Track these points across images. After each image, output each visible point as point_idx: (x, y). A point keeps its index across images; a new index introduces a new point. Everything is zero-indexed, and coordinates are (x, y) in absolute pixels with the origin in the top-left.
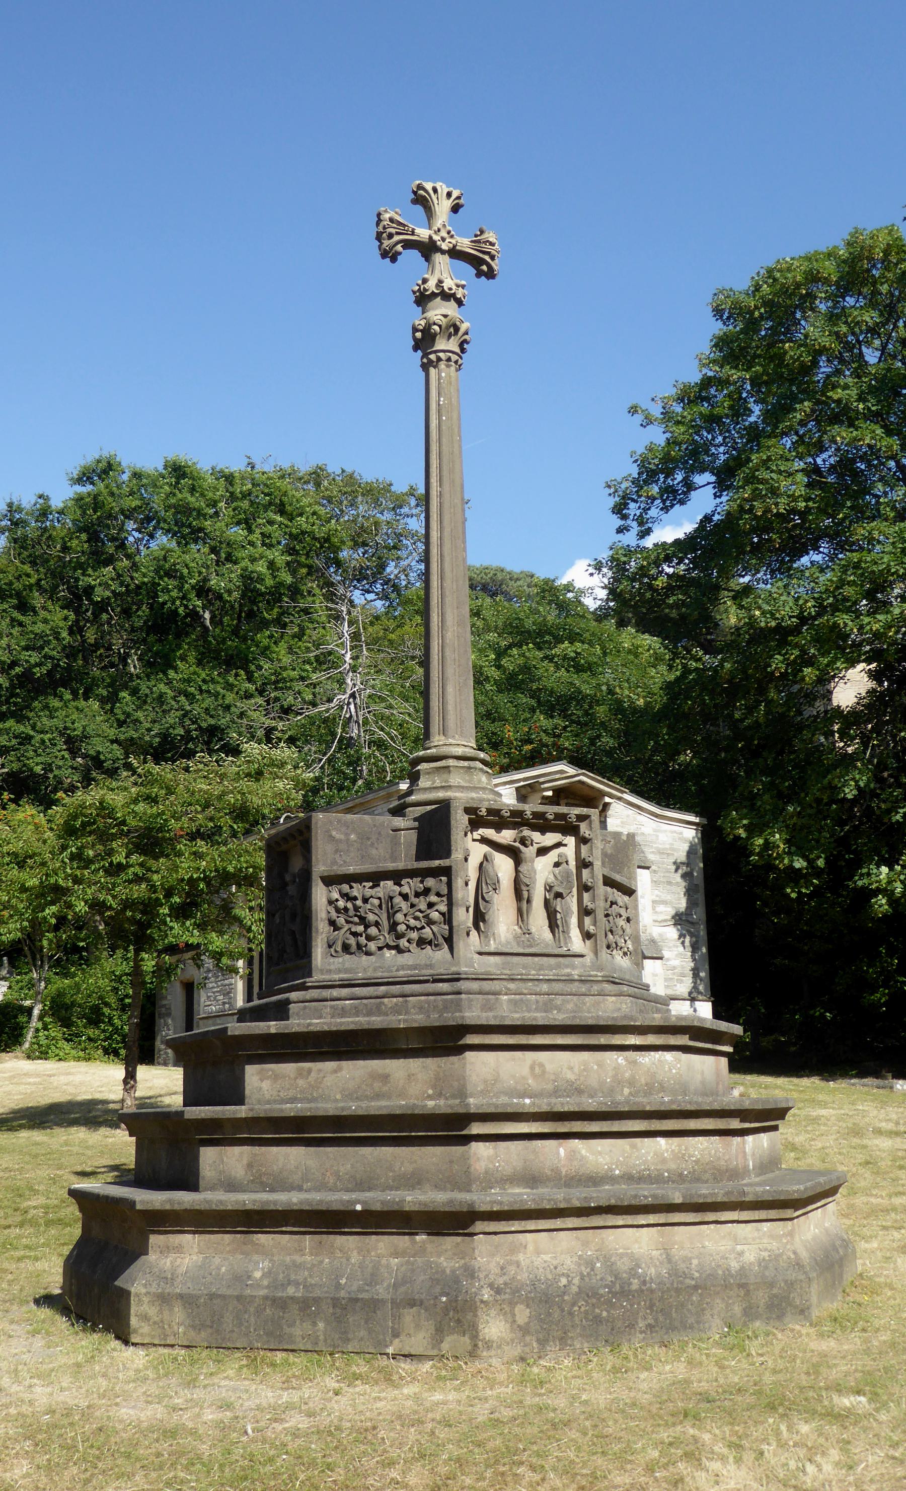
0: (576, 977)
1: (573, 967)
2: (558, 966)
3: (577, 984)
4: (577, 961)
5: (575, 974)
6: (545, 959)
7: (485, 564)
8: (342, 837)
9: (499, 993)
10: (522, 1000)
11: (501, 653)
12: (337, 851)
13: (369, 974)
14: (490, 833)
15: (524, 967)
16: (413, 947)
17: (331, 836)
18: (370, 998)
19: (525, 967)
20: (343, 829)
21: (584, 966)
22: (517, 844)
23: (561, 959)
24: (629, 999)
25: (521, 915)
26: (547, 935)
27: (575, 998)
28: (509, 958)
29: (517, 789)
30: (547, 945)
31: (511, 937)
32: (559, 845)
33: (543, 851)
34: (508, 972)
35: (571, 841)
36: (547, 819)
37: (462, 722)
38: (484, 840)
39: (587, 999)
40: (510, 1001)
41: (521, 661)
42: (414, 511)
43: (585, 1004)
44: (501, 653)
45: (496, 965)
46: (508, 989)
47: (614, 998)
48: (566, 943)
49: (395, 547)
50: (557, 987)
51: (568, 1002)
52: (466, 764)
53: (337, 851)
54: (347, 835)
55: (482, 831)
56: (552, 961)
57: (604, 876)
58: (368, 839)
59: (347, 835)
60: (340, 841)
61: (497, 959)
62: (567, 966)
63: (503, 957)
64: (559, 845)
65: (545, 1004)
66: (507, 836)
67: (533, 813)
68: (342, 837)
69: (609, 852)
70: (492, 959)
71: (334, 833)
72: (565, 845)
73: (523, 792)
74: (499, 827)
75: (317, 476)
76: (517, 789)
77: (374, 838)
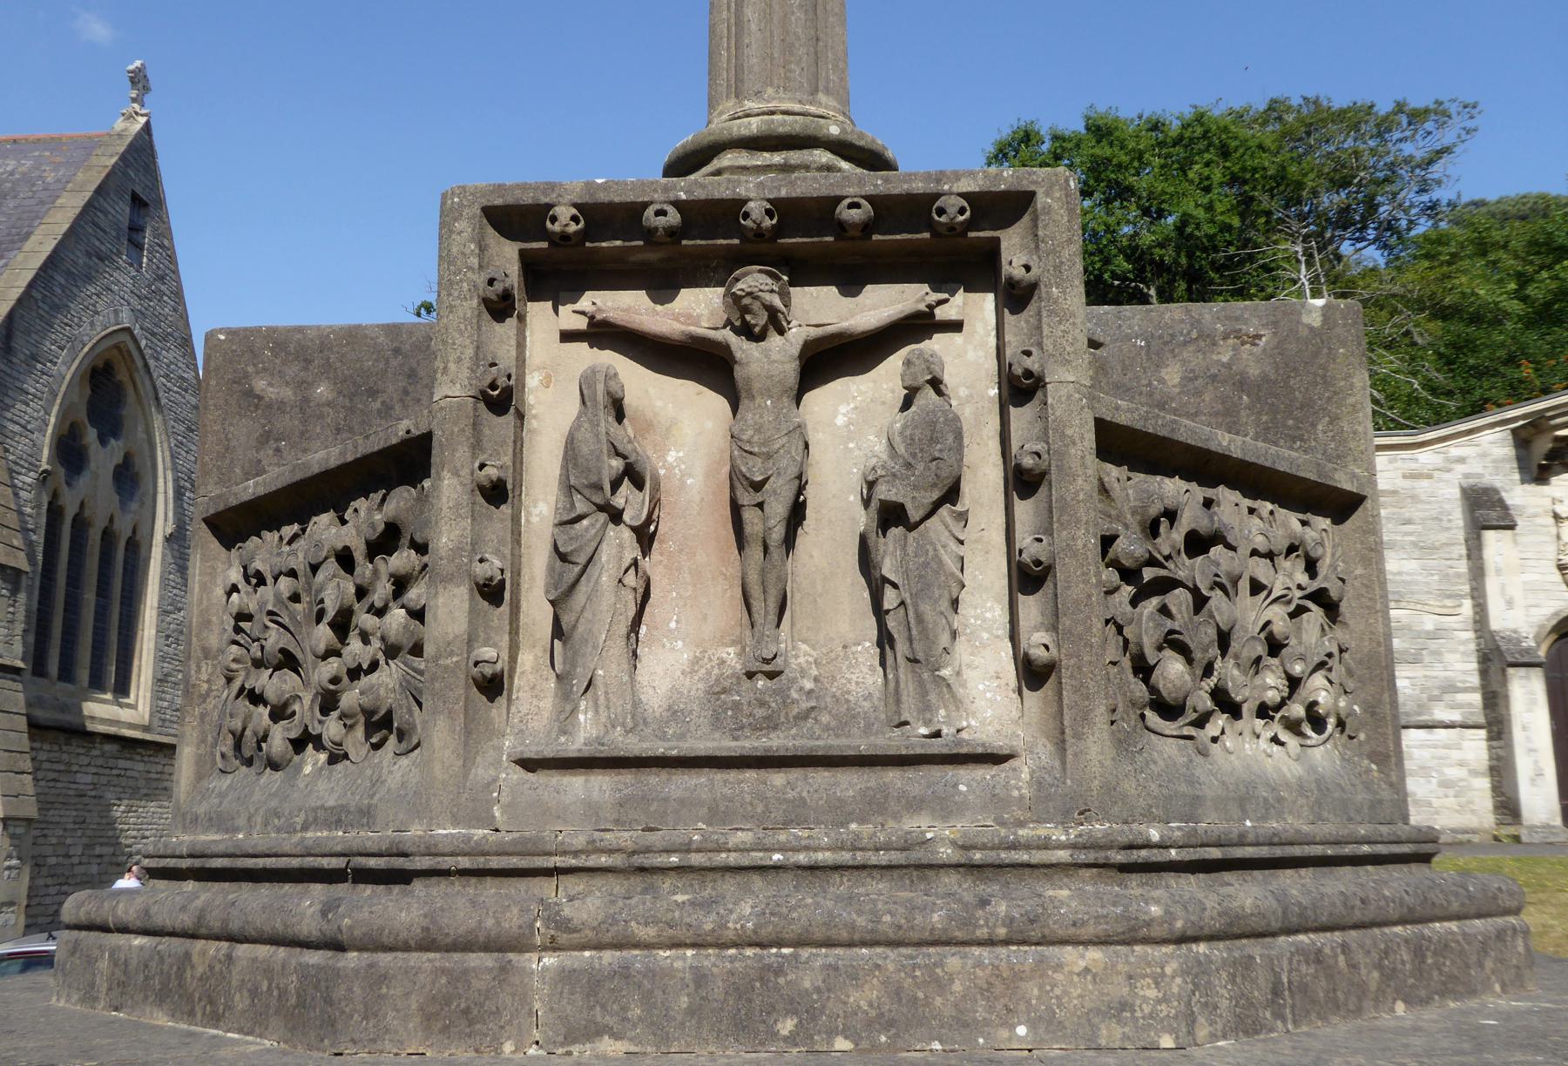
0: (946, 853)
1: (945, 807)
2: (874, 806)
3: (950, 880)
4: (967, 779)
5: (941, 835)
6: (821, 776)
7: (1523, 192)
8: (287, 393)
9: (519, 944)
10: (624, 972)
11: (1523, 280)
12: (265, 438)
13: (258, 839)
14: (628, 306)
15: (716, 815)
16: (356, 742)
17: (250, 393)
18: (173, 934)
19: (716, 815)
20: (293, 370)
21: (997, 801)
22: (727, 335)
23: (892, 775)
24: (1170, 958)
25: (766, 602)
26: (862, 675)
27: (891, 958)
28: (653, 779)
29: (1514, 431)
30: (848, 718)
31: (695, 687)
32: (919, 326)
33: (831, 358)
34: (625, 838)
35: (977, 309)
36: (841, 227)
37: (788, 48)
38: (602, 333)
39: (953, 960)
40: (566, 977)
41: (1554, 285)
42: (1408, 133)
43: (941, 985)
44: (1523, 280)
45: (591, 810)
46: (564, 925)
47: (1094, 955)
48: (926, 709)
49: (1386, 180)
50: (810, 906)
51: (855, 976)
52: (777, 158)
53: (265, 438)
54: (302, 385)
55: (591, 301)
56: (849, 782)
57: (1100, 424)
58: (373, 393)
59: (302, 385)
60: (281, 405)
61: (600, 785)
62: (915, 805)
63: (627, 777)
64: (919, 326)
65: (740, 989)
66: (697, 310)
67: (779, 207)
68: (287, 393)
69: (1254, 371)
70: (576, 785)
71: (260, 385)
72: (956, 326)
73: (1524, 434)
74: (663, 285)
75: (1275, 109)
76: (1514, 431)
77: (391, 389)
